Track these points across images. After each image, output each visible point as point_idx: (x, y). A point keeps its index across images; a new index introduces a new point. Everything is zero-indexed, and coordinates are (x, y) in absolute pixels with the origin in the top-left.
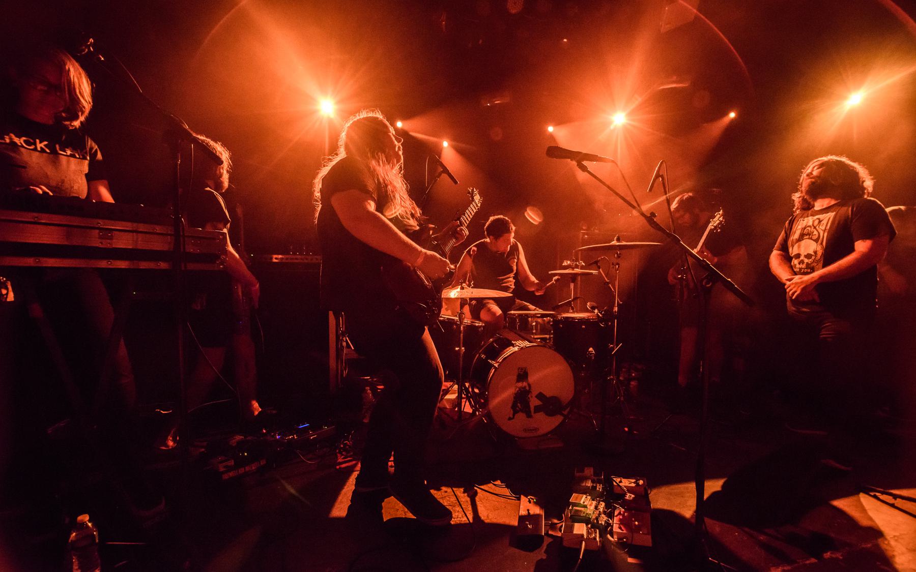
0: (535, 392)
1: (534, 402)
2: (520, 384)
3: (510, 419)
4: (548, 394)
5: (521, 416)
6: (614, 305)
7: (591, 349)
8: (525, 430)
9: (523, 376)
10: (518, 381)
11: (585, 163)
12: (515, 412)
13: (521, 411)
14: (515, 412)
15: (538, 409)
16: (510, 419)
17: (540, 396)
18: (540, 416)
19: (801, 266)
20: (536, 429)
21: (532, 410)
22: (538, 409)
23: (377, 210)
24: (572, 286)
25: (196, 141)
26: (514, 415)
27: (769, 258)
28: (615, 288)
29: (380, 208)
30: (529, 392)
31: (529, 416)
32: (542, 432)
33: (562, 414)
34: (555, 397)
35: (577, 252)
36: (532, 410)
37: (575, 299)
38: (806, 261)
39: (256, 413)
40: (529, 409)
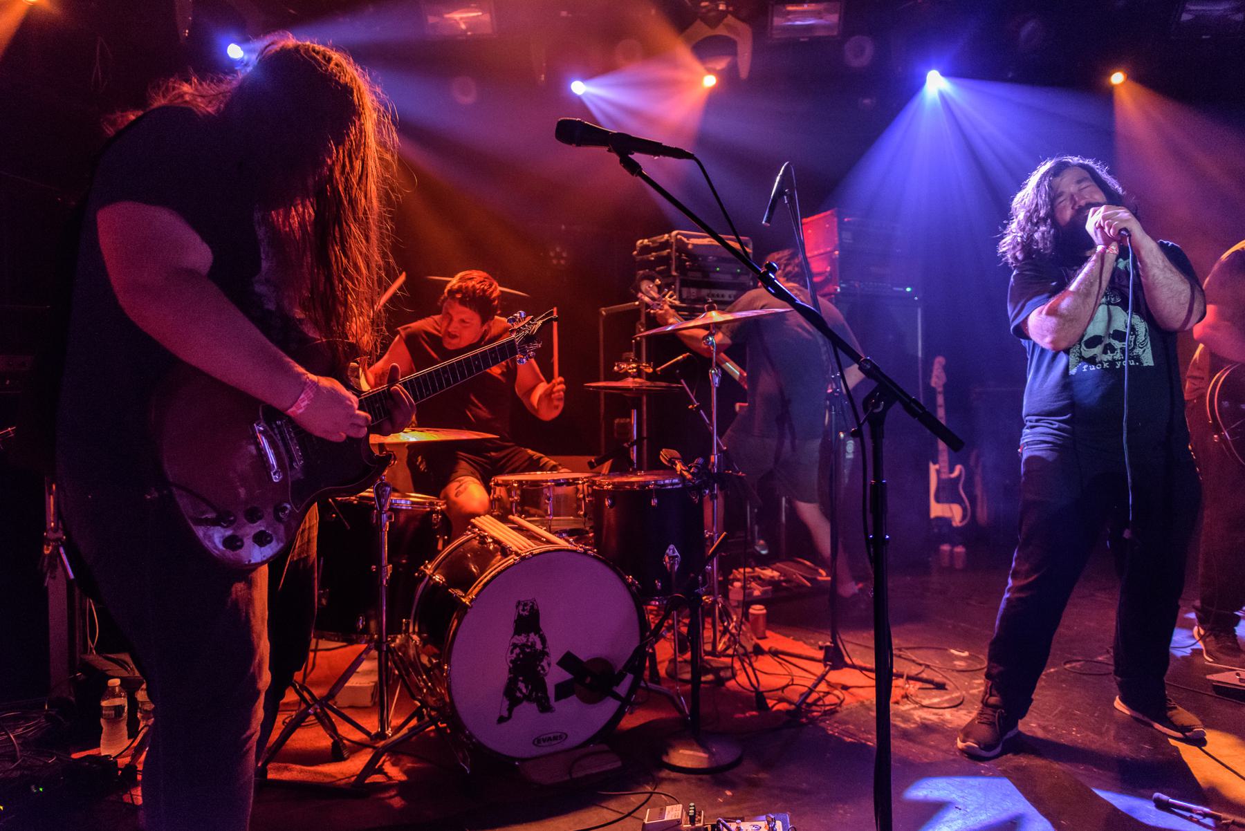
0: (555, 655)
1: (555, 675)
2: (522, 639)
3: (501, 720)
5: (527, 710)
6: (710, 452)
8: (538, 741)
9: (528, 622)
10: (517, 632)
11: (637, 157)
13: (528, 698)
15: (563, 691)
17: (568, 661)
18: (569, 707)
19: (1109, 357)
20: (562, 737)
21: (551, 692)
22: (563, 691)
24: (634, 413)
25: (257, 444)
26: (510, 710)
28: (711, 420)
29: (13, 759)
30: (544, 654)
31: (545, 708)
32: (574, 739)
33: (616, 696)
35: (638, 344)
36: (551, 692)
38: (1117, 344)
40: (544, 690)
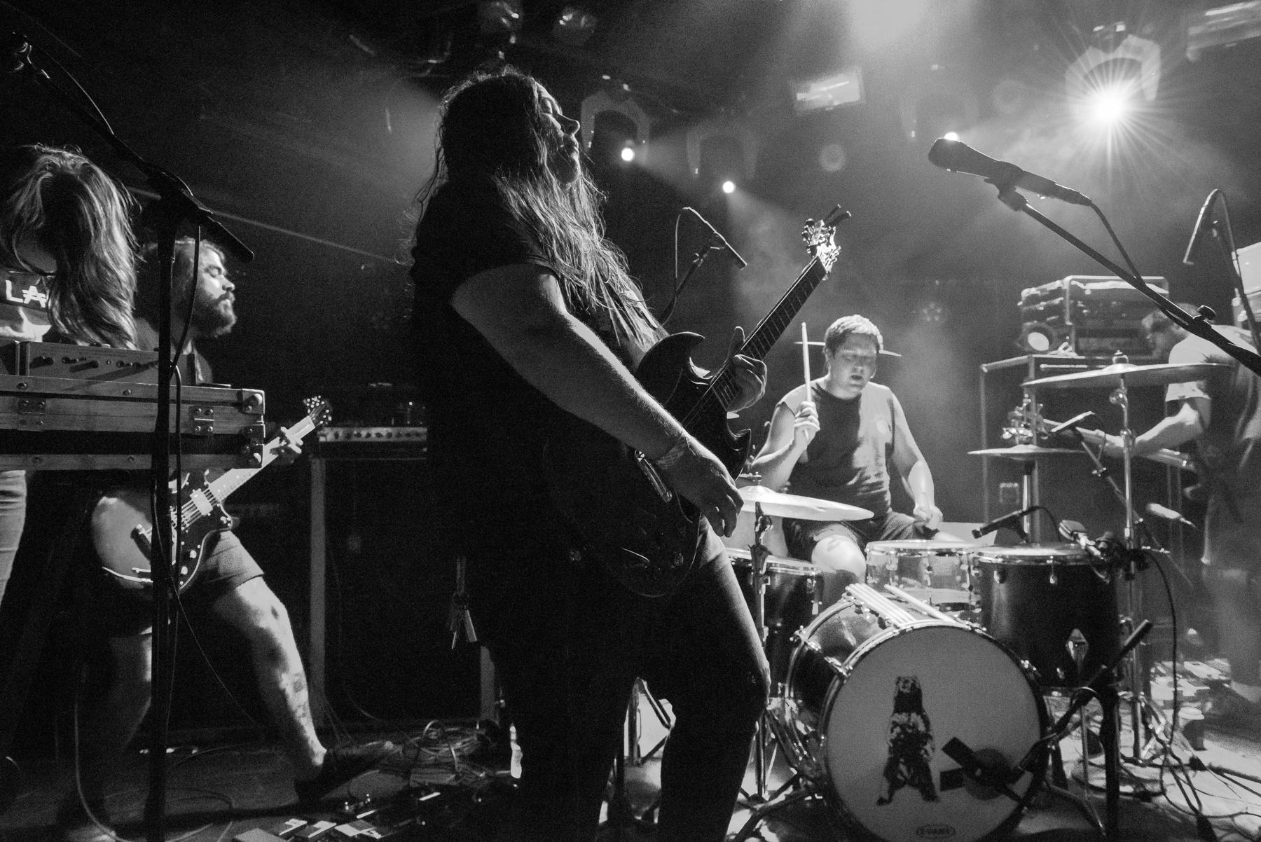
1: (939, 762)
3: (881, 802)
4: (973, 742)
5: (908, 796)
7: (1052, 581)
12: (895, 785)
13: (911, 783)
14: (895, 785)
16: (881, 802)
17: (954, 748)
18: (958, 800)
22: (950, 780)
23: (915, 459)
26: (891, 792)
27: (288, 607)
30: (927, 737)
31: (929, 794)
34: (984, 798)
37: (1031, 510)
39: (319, 761)
